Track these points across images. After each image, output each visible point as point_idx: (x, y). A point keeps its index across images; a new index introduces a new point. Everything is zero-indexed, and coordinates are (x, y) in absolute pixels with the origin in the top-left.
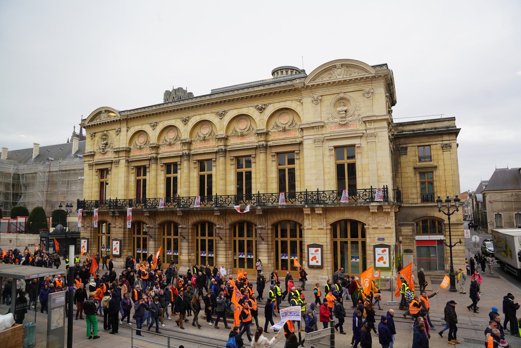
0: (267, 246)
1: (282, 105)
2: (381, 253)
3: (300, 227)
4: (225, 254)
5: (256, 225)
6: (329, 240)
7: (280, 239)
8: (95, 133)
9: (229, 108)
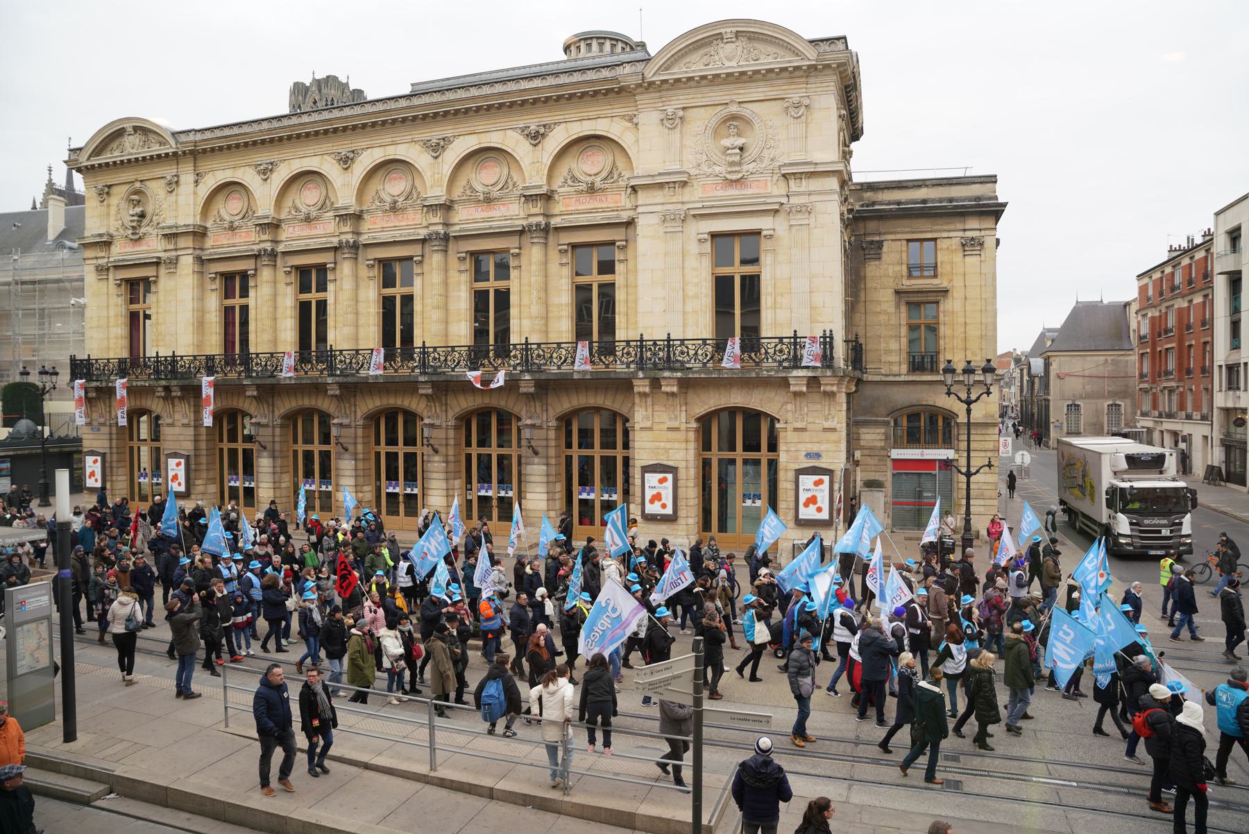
0: (544, 467)
1: (587, 128)
2: (657, 484)
3: (624, 424)
4: (444, 486)
5: (519, 419)
6: (691, 454)
7: (576, 452)
8: (109, 187)
9: (457, 132)
